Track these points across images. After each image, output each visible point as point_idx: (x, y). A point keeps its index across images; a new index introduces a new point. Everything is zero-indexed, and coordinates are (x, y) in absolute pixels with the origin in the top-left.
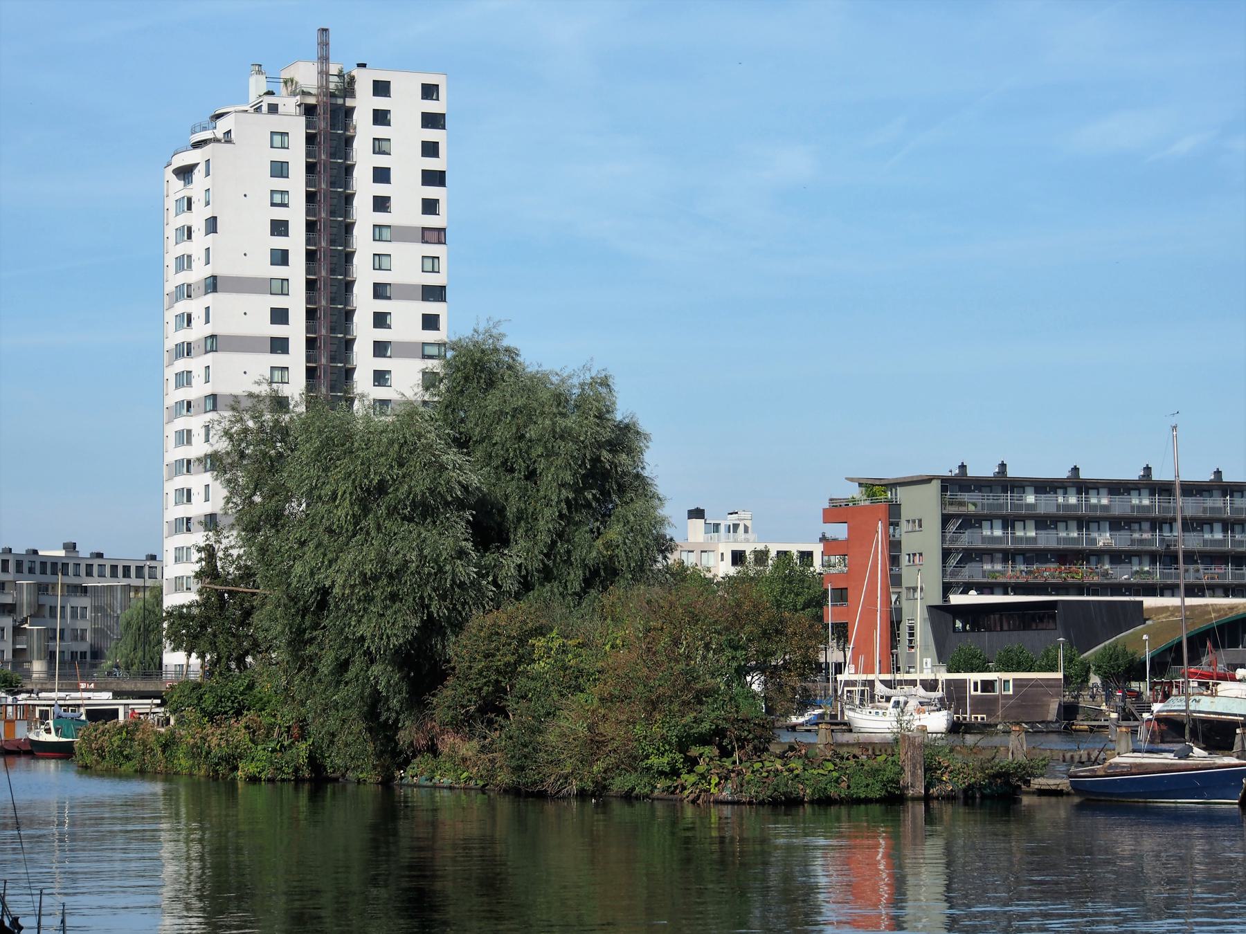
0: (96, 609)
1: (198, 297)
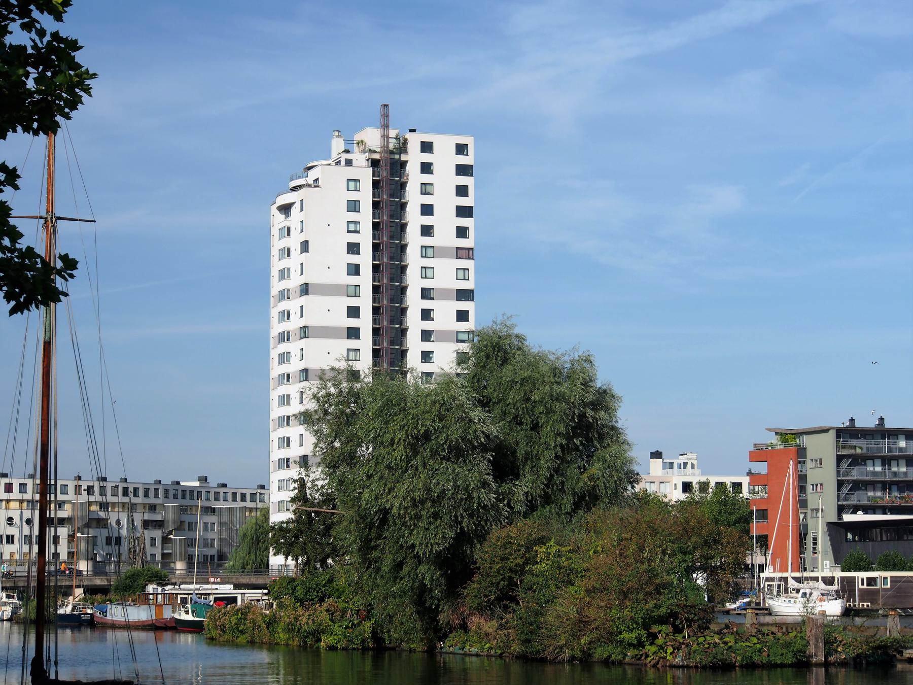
0: (222, 524)
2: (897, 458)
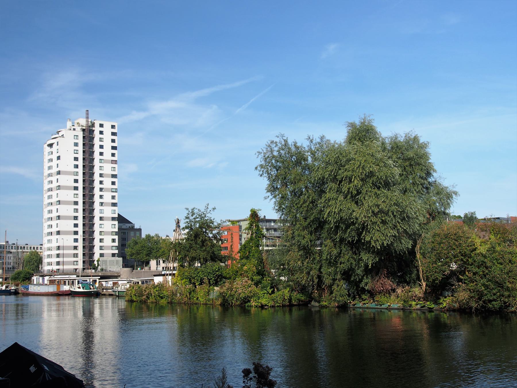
0: (14, 257)
2: (271, 229)
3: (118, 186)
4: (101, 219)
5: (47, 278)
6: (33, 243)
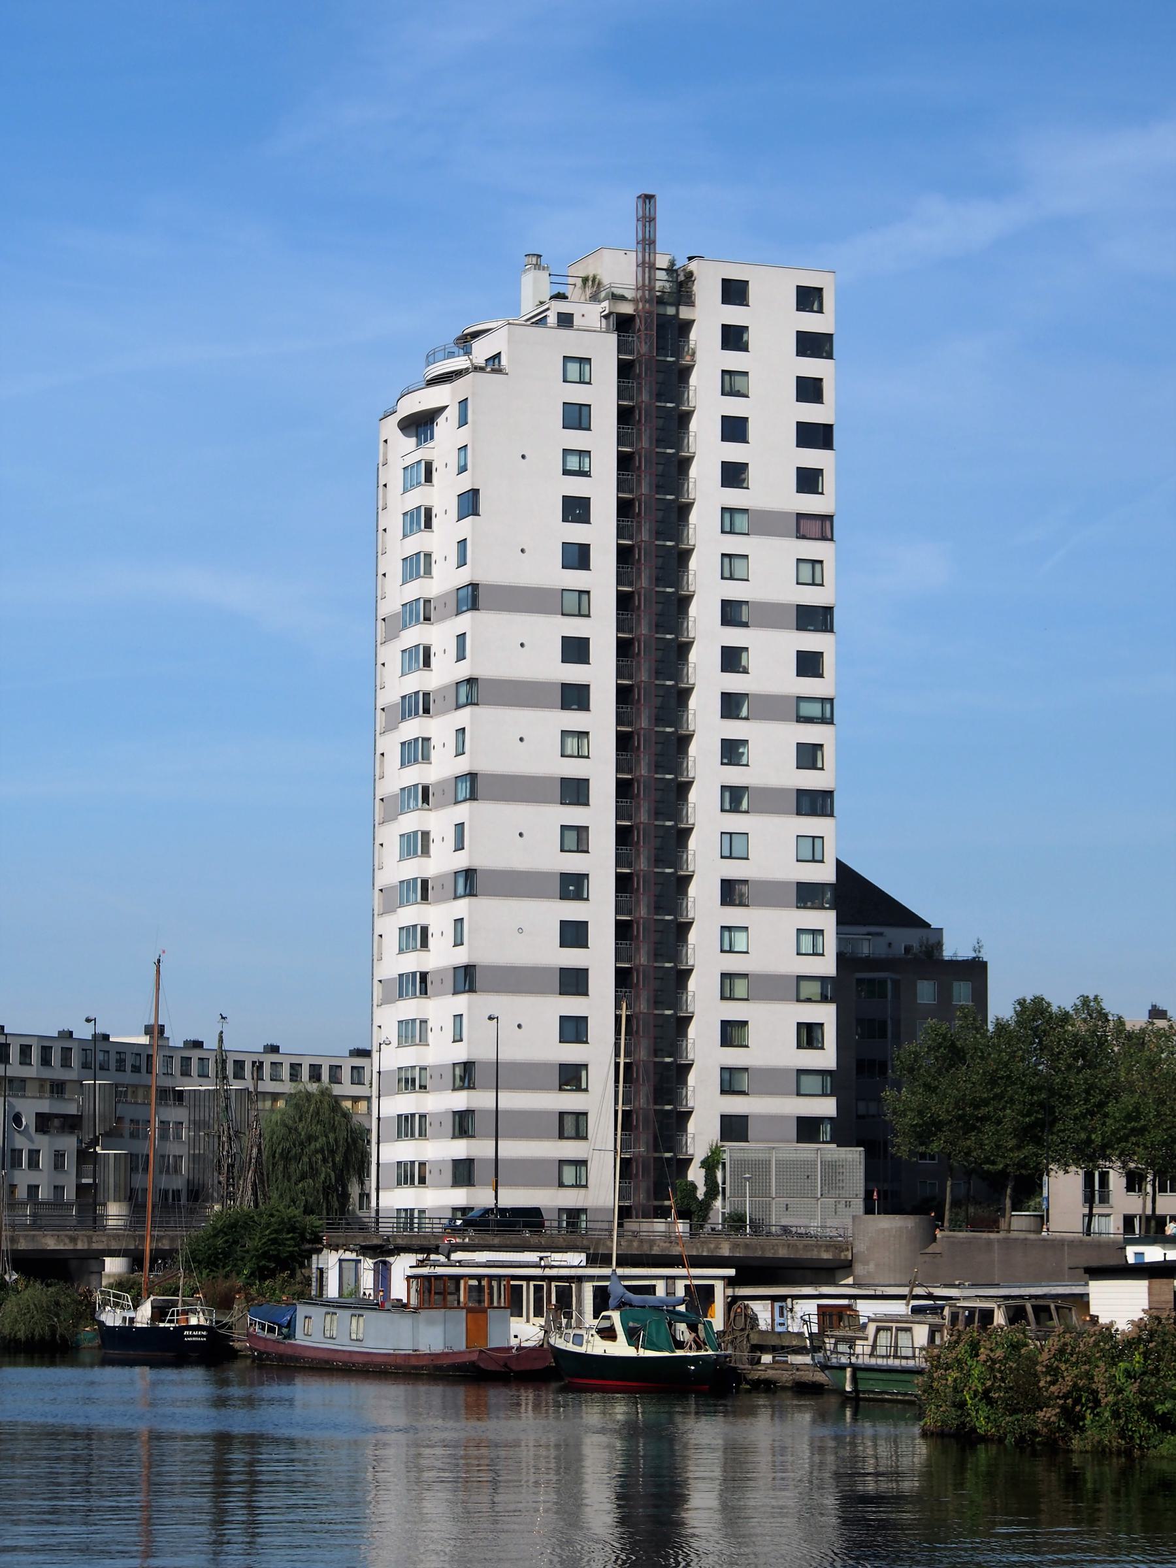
0: (197, 1125)
1: (442, 619)
3: (838, 684)
4: (731, 892)
5: (402, 1266)
6: (311, 1038)
